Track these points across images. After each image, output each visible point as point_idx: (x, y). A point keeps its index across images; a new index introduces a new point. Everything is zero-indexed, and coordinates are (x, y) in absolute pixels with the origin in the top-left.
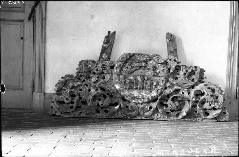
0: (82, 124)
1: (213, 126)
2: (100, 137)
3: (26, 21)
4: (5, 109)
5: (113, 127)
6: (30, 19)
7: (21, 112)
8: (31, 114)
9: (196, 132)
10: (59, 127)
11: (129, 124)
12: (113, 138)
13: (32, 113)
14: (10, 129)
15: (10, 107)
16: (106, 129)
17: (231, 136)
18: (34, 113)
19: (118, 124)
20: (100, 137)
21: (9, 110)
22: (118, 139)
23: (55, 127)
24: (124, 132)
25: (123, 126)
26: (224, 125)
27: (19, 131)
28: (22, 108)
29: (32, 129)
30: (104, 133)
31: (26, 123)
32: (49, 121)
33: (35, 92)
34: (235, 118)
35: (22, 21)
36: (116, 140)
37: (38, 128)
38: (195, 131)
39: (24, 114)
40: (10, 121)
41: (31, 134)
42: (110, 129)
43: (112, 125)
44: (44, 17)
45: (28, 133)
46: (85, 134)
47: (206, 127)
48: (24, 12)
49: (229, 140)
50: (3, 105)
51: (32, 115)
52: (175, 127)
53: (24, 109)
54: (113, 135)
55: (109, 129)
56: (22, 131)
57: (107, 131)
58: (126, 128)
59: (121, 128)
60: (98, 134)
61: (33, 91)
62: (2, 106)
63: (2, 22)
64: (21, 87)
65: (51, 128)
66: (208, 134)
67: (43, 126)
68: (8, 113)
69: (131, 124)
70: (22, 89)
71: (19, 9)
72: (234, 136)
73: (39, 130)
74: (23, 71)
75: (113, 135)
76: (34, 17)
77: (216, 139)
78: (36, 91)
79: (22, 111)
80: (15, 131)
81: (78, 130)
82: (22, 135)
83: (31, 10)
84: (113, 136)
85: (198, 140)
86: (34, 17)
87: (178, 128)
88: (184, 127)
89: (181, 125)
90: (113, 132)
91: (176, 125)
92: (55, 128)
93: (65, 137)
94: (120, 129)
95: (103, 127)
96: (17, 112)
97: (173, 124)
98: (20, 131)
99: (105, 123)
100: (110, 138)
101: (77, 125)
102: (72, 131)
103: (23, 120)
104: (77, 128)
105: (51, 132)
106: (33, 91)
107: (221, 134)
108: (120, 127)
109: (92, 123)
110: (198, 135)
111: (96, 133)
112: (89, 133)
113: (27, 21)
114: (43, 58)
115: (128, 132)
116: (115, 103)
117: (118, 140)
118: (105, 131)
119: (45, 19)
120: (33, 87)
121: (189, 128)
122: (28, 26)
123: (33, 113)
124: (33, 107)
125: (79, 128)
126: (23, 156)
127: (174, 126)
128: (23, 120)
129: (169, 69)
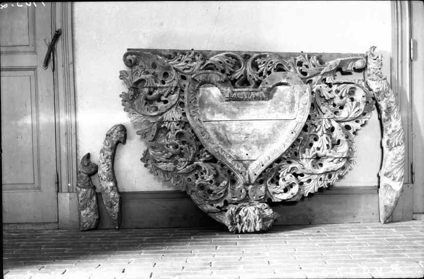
0: (148, 245)
1: (376, 234)
2: (183, 268)
3: (41, 69)
4: (10, 225)
5: (204, 248)
6: (46, 64)
7: (37, 229)
8: (58, 231)
9: (346, 247)
10: (110, 254)
11: (230, 240)
12: (205, 268)
13: (58, 229)
14: (25, 263)
15: (19, 222)
16: (191, 252)
17: (408, 251)
18: (62, 229)
19: (212, 241)
20: (183, 268)
21: (18, 226)
22: (215, 268)
23: (104, 254)
24: (223, 255)
25: (221, 244)
26: (394, 230)
27: (41, 266)
28: (40, 221)
29: (64, 261)
30: (191, 259)
31: (51, 251)
32: (90, 243)
33: (61, 192)
34: (412, 216)
35: (34, 69)
36: (212, 272)
37: (74, 258)
38: (346, 244)
39: (46, 232)
40: (24, 247)
41: (64, 270)
42: (198, 251)
43: (200, 244)
44: (71, 60)
45: (57, 269)
46: (157, 264)
47: (364, 237)
48: (35, 52)
49: (404, 260)
50: (6, 219)
51: (59, 233)
52: (311, 240)
53: (44, 223)
54: (205, 262)
55: (197, 251)
56: (45, 266)
57: (194, 255)
58: (227, 247)
59: (218, 248)
60: (180, 262)
61: (58, 192)
62: (5, 220)
63: (3, 73)
64: (36, 185)
65: (95, 256)
66: (369, 250)
67: (82, 254)
68: (16, 233)
69: (233, 240)
70: (39, 188)
71: (27, 49)
72: (412, 251)
73: (76, 261)
74: (38, 155)
75: (205, 262)
76: (53, 60)
77: (382, 259)
78: (63, 191)
79: (42, 227)
80: (34, 266)
81: (144, 256)
82: (47, 272)
83: (47, 49)
84: (205, 264)
85: (352, 262)
86: (53, 60)
87: (316, 242)
88: (325, 238)
89: (321, 235)
90: (205, 257)
91: (313, 236)
92: (103, 256)
93: (123, 272)
94: (214, 249)
95: (185, 248)
96: (32, 230)
97: (306, 235)
98: (43, 265)
99: (189, 241)
100: (201, 268)
101: (140, 249)
102: (133, 260)
103: (44, 244)
104: (142, 254)
105: (97, 264)
106: (58, 192)
107: (391, 250)
108: (217, 247)
109: (166, 242)
110: (352, 253)
111: (176, 260)
112: (164, 262)
113: (43, 69)
114: (74, 131)
115: (229, 254)
116: (198, 177)
117: (214, 271)
118: (190, 256)
119: (73, 63)
120: (58, 183)
121: (335, 241)
122: (45, 75)
123: (61, 229)
124: (61, 217)
125: (145, 253)
126: (305, 277)
127: (309, 237)
128: (44, 244)
129: (321, 70)
